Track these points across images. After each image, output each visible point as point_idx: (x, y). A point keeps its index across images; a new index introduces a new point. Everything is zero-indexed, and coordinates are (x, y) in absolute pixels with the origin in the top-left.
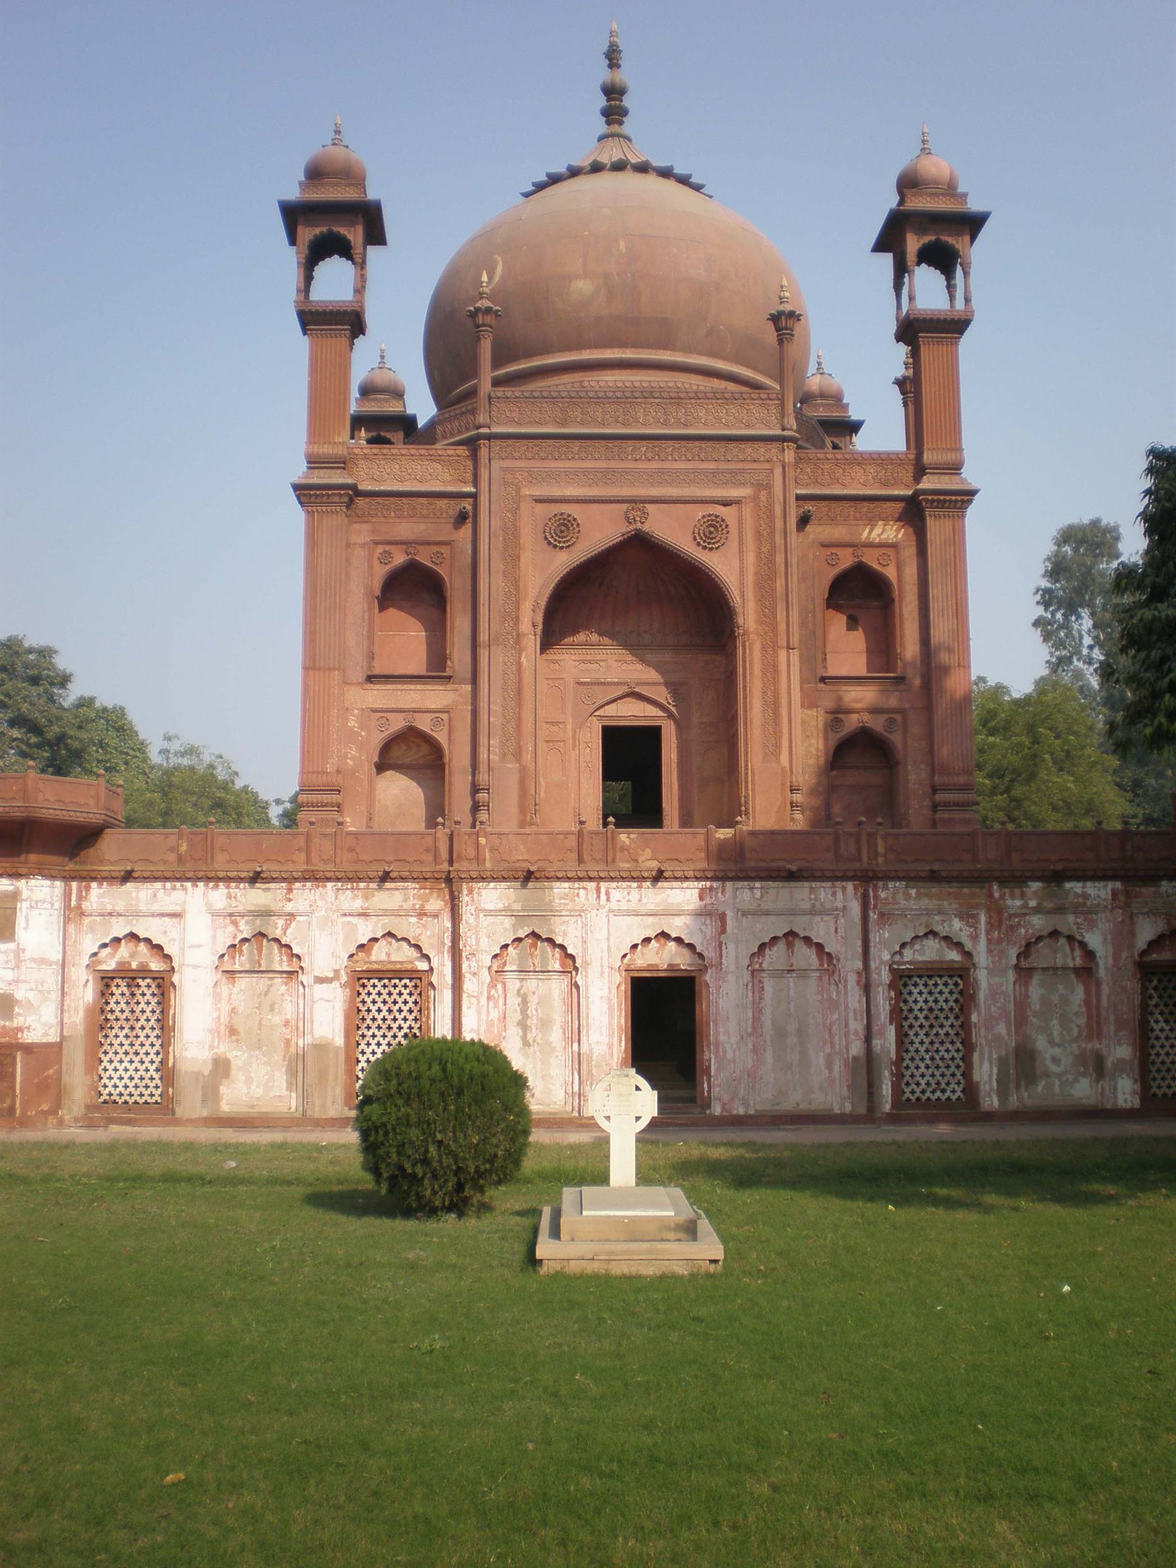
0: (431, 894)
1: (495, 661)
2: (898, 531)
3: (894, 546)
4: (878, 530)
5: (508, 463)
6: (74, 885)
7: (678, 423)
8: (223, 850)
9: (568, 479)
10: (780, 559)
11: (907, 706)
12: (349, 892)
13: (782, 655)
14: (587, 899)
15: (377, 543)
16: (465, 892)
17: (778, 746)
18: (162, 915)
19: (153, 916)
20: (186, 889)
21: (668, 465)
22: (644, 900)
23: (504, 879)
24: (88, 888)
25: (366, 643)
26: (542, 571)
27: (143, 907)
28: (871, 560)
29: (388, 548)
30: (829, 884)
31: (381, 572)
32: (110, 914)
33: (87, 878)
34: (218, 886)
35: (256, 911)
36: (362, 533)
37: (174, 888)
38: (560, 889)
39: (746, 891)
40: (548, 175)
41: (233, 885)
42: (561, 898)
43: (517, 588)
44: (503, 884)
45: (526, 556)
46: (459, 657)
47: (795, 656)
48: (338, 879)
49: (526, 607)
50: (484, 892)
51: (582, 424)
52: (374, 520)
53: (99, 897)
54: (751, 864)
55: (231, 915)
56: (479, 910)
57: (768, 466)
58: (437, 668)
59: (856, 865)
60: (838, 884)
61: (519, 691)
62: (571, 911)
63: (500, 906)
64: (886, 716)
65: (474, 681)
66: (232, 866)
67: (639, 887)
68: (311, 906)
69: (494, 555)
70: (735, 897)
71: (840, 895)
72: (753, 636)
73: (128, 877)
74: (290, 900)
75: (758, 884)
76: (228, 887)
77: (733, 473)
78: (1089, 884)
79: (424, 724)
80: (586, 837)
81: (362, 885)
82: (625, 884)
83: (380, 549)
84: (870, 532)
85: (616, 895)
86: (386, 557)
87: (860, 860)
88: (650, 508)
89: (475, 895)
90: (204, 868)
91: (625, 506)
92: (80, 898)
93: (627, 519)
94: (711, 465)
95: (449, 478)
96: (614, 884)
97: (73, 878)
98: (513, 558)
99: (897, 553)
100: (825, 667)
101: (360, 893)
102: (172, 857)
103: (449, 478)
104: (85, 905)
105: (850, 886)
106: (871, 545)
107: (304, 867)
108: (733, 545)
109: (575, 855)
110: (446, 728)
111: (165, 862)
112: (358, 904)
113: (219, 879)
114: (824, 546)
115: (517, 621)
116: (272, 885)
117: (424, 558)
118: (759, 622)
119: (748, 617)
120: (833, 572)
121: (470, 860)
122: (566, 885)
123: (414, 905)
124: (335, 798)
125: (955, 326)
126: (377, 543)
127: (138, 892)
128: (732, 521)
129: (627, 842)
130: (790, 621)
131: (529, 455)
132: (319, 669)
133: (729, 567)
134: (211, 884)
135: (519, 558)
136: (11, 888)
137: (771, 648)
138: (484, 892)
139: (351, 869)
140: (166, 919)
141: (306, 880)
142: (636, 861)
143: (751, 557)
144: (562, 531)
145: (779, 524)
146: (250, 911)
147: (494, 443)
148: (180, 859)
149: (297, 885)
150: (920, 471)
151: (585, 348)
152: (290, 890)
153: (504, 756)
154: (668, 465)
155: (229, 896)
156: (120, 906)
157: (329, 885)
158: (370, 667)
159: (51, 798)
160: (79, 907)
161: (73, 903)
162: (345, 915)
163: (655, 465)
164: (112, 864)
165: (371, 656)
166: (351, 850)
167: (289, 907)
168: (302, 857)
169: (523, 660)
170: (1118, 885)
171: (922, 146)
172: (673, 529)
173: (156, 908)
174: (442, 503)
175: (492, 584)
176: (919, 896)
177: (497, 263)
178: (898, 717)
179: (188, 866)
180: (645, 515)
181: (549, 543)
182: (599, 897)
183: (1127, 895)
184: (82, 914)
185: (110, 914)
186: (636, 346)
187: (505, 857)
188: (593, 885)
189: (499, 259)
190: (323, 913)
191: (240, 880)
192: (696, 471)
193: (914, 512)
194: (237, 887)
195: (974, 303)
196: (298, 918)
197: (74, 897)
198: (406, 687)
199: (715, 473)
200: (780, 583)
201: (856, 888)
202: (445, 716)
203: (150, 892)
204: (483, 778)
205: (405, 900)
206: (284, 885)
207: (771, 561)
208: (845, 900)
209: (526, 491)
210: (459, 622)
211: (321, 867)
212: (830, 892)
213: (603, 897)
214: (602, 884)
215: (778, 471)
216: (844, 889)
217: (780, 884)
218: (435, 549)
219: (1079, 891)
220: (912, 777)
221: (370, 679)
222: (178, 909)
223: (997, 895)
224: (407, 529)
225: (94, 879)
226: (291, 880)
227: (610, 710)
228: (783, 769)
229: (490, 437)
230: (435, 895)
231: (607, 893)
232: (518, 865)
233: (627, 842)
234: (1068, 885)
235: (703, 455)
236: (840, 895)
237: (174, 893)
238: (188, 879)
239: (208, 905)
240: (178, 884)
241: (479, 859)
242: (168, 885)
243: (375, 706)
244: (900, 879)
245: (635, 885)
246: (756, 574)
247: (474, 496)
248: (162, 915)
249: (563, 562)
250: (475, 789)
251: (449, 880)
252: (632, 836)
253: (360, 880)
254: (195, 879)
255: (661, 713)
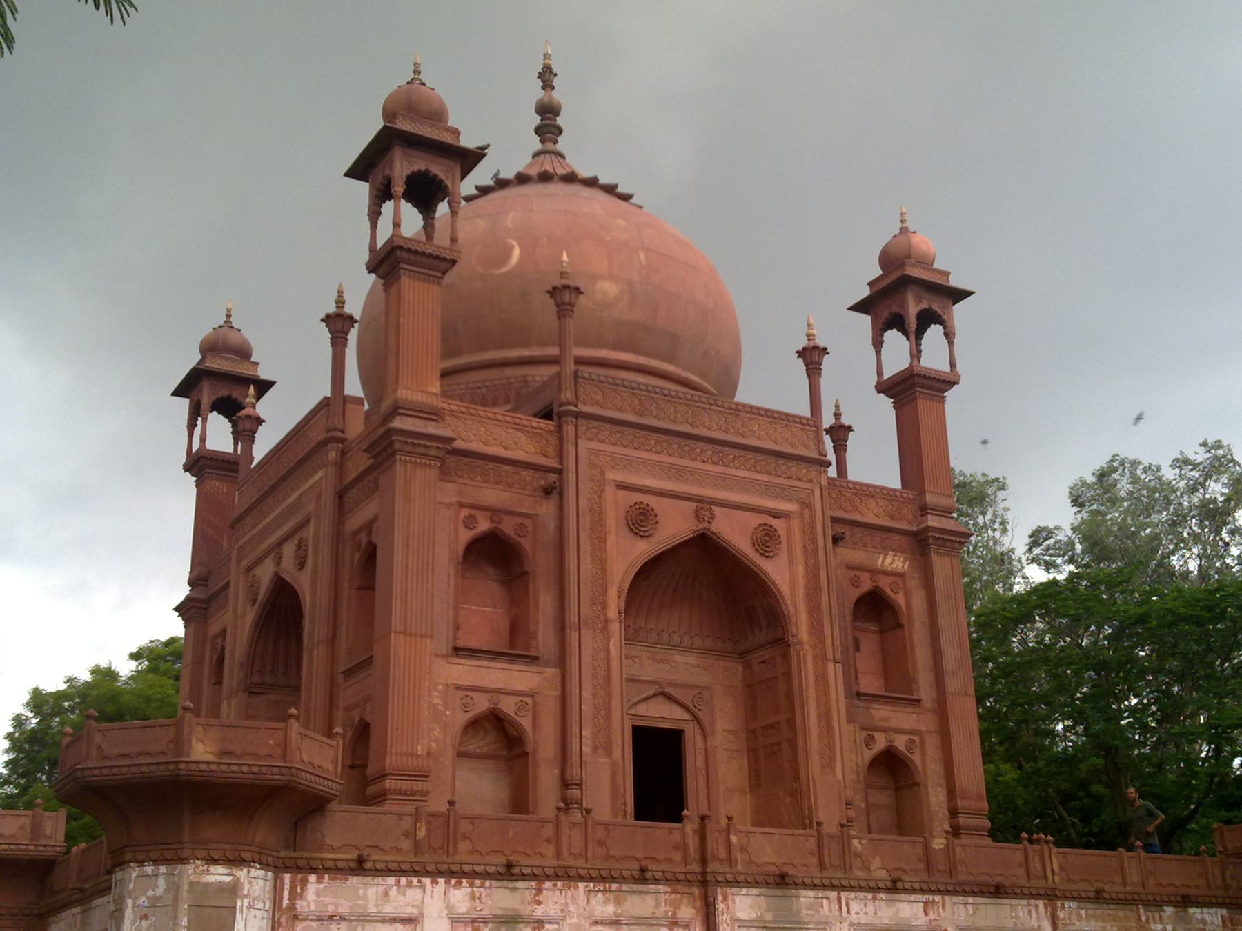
0: (681, 900)
1: (587, 644)
2: (904, 562)
3: (901, 575)
4: (889, 560)
5: (594, 445)
6: (287, 877)
7: (737, 433)
8: (466, 837)
9: (647, 469)
10: (823, 575)
11: (923, 728)
12: (600, 895)
13: (831, 666)
14: (830, 911)
15: (462, 505)
16: (720, 898)
17: (832, 759)
18: (394, 920)
19: (383, 921)
20: (423, 887)
21: (732, 471)
22: (879, 914)
23: (756, 884)
24: (304, 882)
25: (451, 612)
26: (626, 555)
27: (372, 909)
28: (885, 584)
29: (474, 512)
30: (1024, 902)
31: (466, 536)
32: (331, 918)
33: (302, 868)
34: (461, 883)
35: (502, 917)
36: (449, 492)
37: (410, 885)
38: (806, 897)
39: (962, 907)
40: (477, 188)
41: (478, 882)
42: (808, 909)
43: (604, 571)
44: (755, 891)
45: (611, 539)
46: (545, 639)
47: (839, 667)
48: (591, 879)
49: (613, 593)
50: (737, 899)
51: (657, 417)
52: (460, 480)
53: (318, 894)
54: (962, 877)
55: (474, 921)
56: (735, 920)
57: (808, 486)
58: (515, 646)
59: (1042, 883)
60: (1032, 901)
61: (608, 678)
62: (816, 923)
63: (754, 916)
64: (908, 737)
65: (562, 662)
66: (476, 858)
67: (874, 898)
68: (562, 911)
69: (583, 535)
70: (953, 913)
71: (1034, 915)
72: (806, 647)
73: (360, 867)
74: (539, 903)
75: (970, 900)
76: (472, 885)
77: (783, 488)
78: (1205, 910)
79: (508, 706)
80: (825, 839)
81: (614, 886)
82: (862, 895)
83: (464, 512)
84: (884, 560)
85: (855, 906)
86: (470, 523)
87: (1046, 878)
88: (716, 509)
89: (730, 902)
90: (445, 858)
91: (694, 505)
92: (293, 896)
93: (697, 516)
94: (764, 477)
95: (533, 450)
96: (852, 895)
97: (286, 869)
98: (600, 541)
99: (904, 582)
100: (858, 684)
101: (612, 896)
102: (406, 844)
103: (533, 450)
104: (300, 905)
105: (1041, 903)
106: (885, 573)
107: (555, 863)
108: (783, 558)
109: (814, 860)
110: (530, 714)
111: (399, 850)
112: (610, 909)
113: (464, 874)
114: (850, 567)
115: (604, 605)
116: (520, 884)
117: (508, 527)
118: (810, 634)
119: (801, 627)
120: (857, 593)
121: (721, 861)
122: (811, 893)
123: (666, 912)
124: (417, 786)
125: (941, 384)
126: (462, 505)
127: (366, 890)
128: (781, 532)
129: (859, 848)
130: (833, 634)
131: (613, 440)
132: (411, 635)
133: (784, 574)
134: (453, 881)
135: (605, 541)
136: (228, 879)
137: (821, 659)
138: (737, 899)
139: (606, 866)
140: (398, 925)
141: (557, 877)
142: (868, 869)
143: (800, 570)
144: (640, 521)
145: (820, 542)
146: (496, 916)
147: (582, 422)
148: (417, 847)
149: (548, 884)
150: (924, 510)
151: (602, 348)
152: (539, 891)
153: (595, 749)
154: (732, 471)
155: (473, 897)
156: (344, 908)
157: (581, 885)
158: (455, 638)
159: (306, 759)
160: (292, 907)
161: (285, 902)
162: (597, 923)
163: (719, 469)
164: (333, 850)
165: (457, 628)
166: (601, 843)
167: (539, 912)
168: (549, 850)
169: (612, 647)
170: (1224, 912)
171: (900, 225)
172: (735, 532)
173: (388, 910)
174: (527, 474)
175: (581, 565)
176: (1088, 917)
177: (512, 247)
178: (916, 738)
179: (427, 857)
180: (713, 517)
181: (631, 529)
182: (840, 908)
183: (1232, 920)
184: (295, 918)
185: (331, 918)
186: (647, 355)
187: (754, 858)
188: (833, 895)
189: (515, 243)
190: (575, 920)
191: (486, 876)
192: (753, 482)
193: (921, 544)
194: (482, 886)
195: (959, 368)
196: (548, 926)
197: (286, 894)
198: (492, 664)
199: (768, 486)
200: (825, 598)
201: (1046, 908)
202: (528, 700)
203: (381, 889)
204: (574, 772)
205: (657, 906)
206: (533, 883)
207: (817, 576)
208: (1038, 918)
209: (610, 476)
210: (544, 603)
211: (571, 862)
212: (1026, 910)
213: (844, 908)
214: (844, 895)
215: (817, 493)
216: (1037, 907)
217: (987, 900)
218: (519, 520)
219: (1199, 916)
220: (933, 799)
221: (458, 651)
222: (410, 911)
223: (1143, 919)
224: (491, 495)
225: (313, 870)
226: (539, 877)
227: (641, 709)
228: (839, 782)
229: (577, 415)
230: (685, 900)
231: (847, 905)
232: (766, 868)
233: (859, 848)
234: (1191, 910)
235: (758, 468)
236: (1034, 915)
237: (410, 892)
238: (428, 874)
239: (449, 907)
240: (415, 880)
241: (730, 861)
242: (403, 880)
243: (460, 683)
244: (1074, 899)
245: (870, 896)
246: (806, 587)
247: (559, 472)
248: (394, 920)
249: (643, 550)
250: (565, 784)
251: (704, 883)
252: (864, 842)
253: (613, 879)
254: (435, 874)
255: (687, 716)
